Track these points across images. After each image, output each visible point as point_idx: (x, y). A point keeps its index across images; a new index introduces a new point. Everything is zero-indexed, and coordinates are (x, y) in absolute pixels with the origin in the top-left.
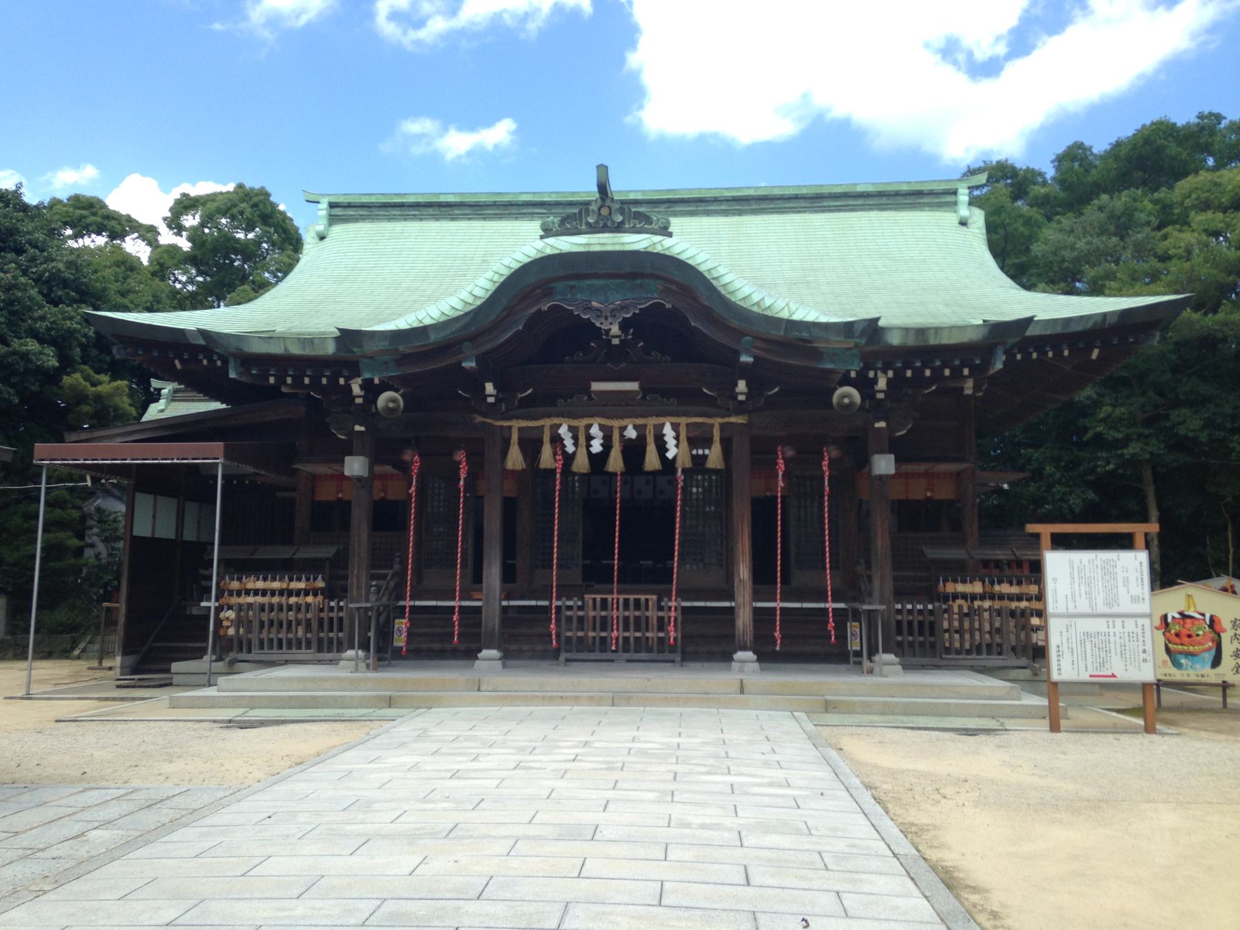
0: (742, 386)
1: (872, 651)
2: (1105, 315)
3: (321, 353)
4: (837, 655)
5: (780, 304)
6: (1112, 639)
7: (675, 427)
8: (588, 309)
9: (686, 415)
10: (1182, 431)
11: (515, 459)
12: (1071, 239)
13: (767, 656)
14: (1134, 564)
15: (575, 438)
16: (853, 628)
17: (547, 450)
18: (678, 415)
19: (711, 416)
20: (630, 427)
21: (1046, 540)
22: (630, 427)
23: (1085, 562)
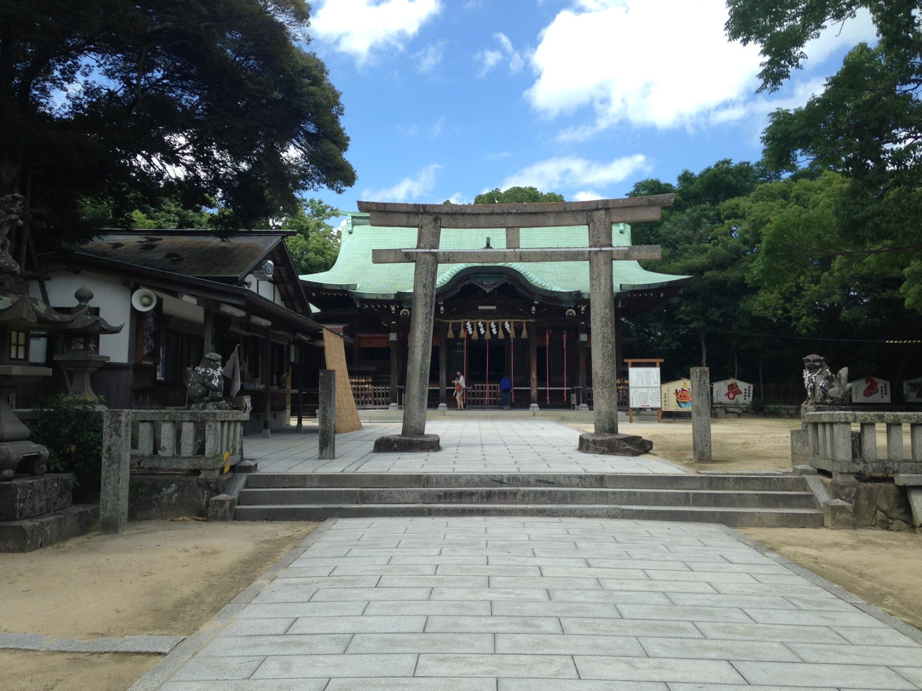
0: (534, 309)
1: (578, 404)
4: (568, 406)
5: (548, 285)
7: (509, 323)
8: (482, 284)
10: (711, 317)
11: (450, 334)
12: (675, 229)
13: (543, 406)
14: (655, 372)
15: (472, 327)
16: (574, 396)
17: (462, 331)
21: (630, 364)
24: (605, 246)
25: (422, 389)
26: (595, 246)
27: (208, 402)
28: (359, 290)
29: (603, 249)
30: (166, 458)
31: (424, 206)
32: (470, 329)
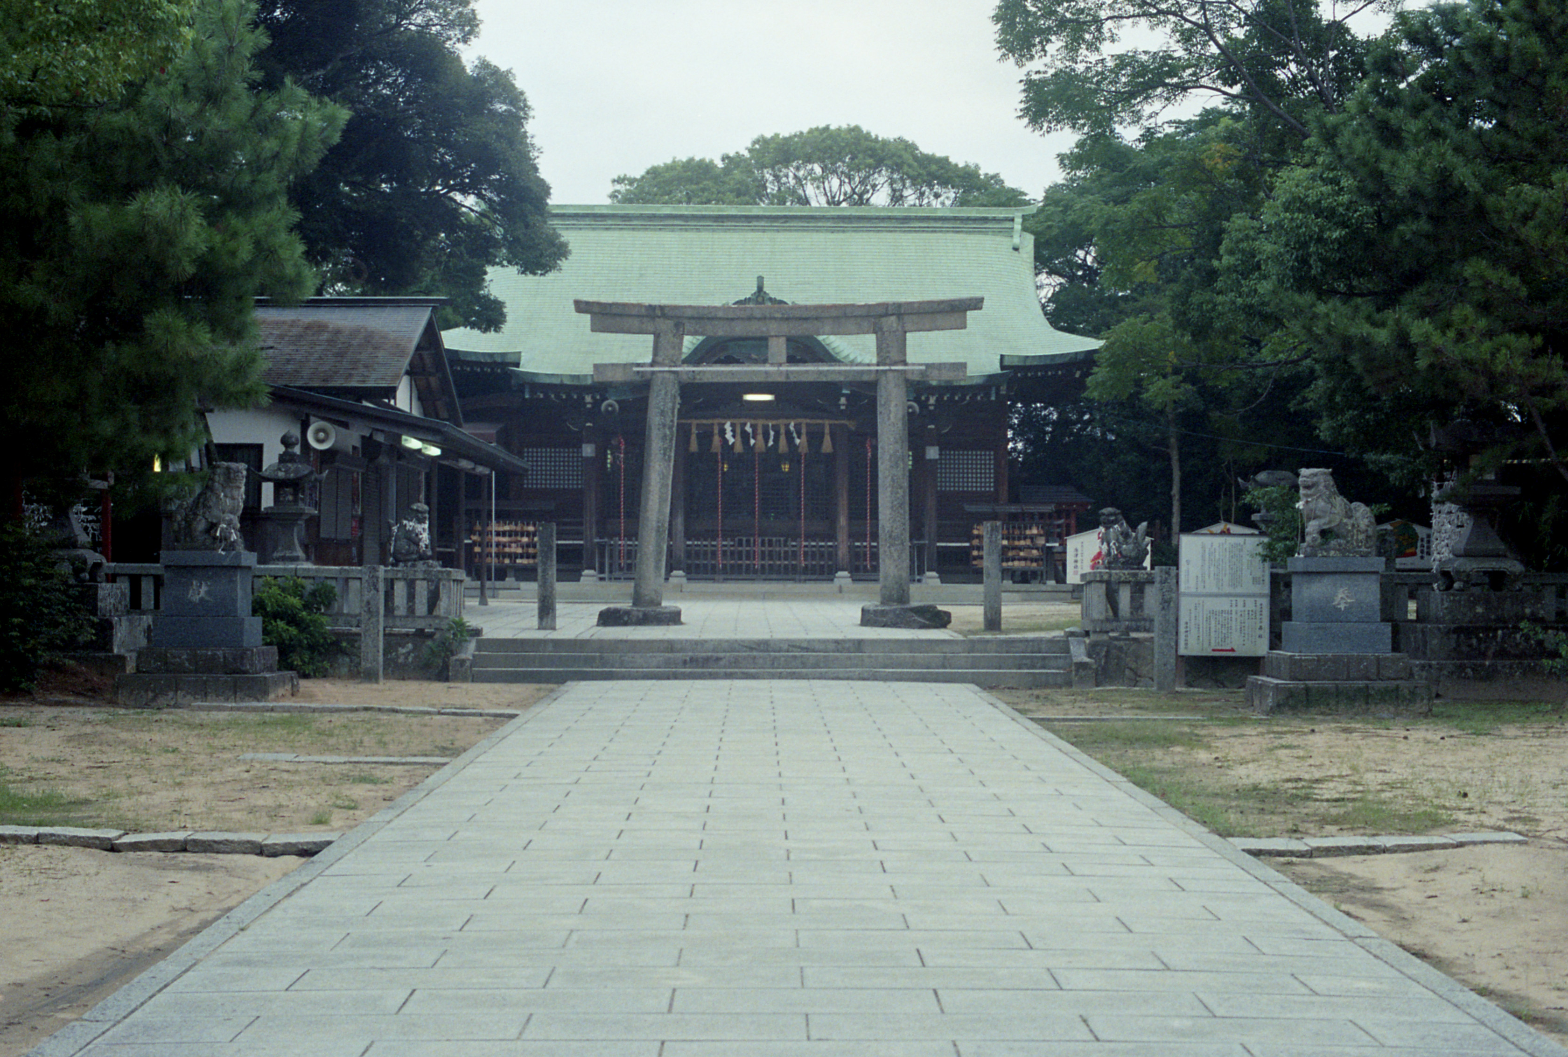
0: (843, 400)
2: (1076, 353)
3: (584, 383)
6: (1234, 616)
9: (805, 417)
17: (716, 439)
18: (735, 417)
19: (822, 418)
20: (749, 424)
22: (749, 424)
23: (1216, 545)
24: (895, 363)
25: (659, 546)
26: (885, 364)
27: (415, 560)
28: (527, 366)
29: (893, 368)
30: (400, 617)
31: (662, 308)
32: (729, 435)
